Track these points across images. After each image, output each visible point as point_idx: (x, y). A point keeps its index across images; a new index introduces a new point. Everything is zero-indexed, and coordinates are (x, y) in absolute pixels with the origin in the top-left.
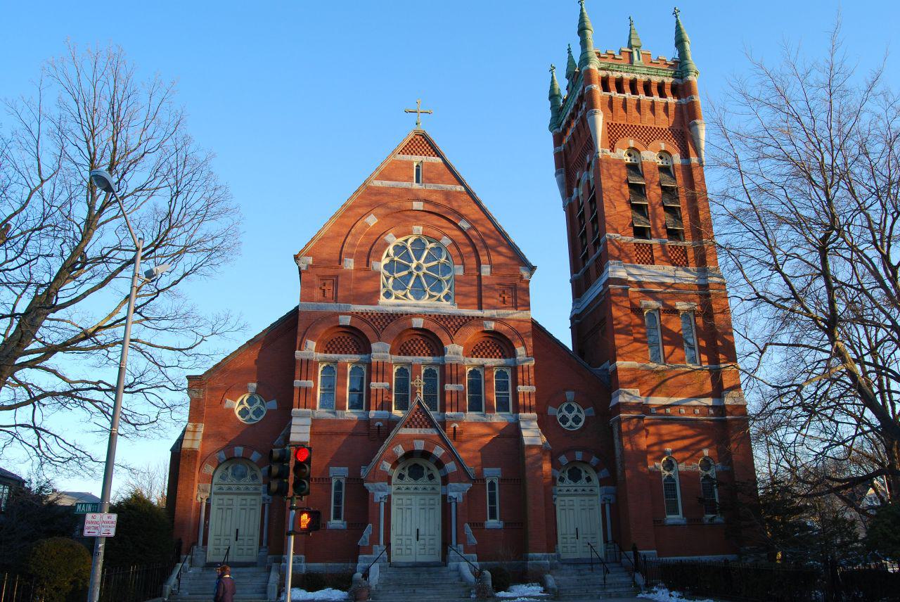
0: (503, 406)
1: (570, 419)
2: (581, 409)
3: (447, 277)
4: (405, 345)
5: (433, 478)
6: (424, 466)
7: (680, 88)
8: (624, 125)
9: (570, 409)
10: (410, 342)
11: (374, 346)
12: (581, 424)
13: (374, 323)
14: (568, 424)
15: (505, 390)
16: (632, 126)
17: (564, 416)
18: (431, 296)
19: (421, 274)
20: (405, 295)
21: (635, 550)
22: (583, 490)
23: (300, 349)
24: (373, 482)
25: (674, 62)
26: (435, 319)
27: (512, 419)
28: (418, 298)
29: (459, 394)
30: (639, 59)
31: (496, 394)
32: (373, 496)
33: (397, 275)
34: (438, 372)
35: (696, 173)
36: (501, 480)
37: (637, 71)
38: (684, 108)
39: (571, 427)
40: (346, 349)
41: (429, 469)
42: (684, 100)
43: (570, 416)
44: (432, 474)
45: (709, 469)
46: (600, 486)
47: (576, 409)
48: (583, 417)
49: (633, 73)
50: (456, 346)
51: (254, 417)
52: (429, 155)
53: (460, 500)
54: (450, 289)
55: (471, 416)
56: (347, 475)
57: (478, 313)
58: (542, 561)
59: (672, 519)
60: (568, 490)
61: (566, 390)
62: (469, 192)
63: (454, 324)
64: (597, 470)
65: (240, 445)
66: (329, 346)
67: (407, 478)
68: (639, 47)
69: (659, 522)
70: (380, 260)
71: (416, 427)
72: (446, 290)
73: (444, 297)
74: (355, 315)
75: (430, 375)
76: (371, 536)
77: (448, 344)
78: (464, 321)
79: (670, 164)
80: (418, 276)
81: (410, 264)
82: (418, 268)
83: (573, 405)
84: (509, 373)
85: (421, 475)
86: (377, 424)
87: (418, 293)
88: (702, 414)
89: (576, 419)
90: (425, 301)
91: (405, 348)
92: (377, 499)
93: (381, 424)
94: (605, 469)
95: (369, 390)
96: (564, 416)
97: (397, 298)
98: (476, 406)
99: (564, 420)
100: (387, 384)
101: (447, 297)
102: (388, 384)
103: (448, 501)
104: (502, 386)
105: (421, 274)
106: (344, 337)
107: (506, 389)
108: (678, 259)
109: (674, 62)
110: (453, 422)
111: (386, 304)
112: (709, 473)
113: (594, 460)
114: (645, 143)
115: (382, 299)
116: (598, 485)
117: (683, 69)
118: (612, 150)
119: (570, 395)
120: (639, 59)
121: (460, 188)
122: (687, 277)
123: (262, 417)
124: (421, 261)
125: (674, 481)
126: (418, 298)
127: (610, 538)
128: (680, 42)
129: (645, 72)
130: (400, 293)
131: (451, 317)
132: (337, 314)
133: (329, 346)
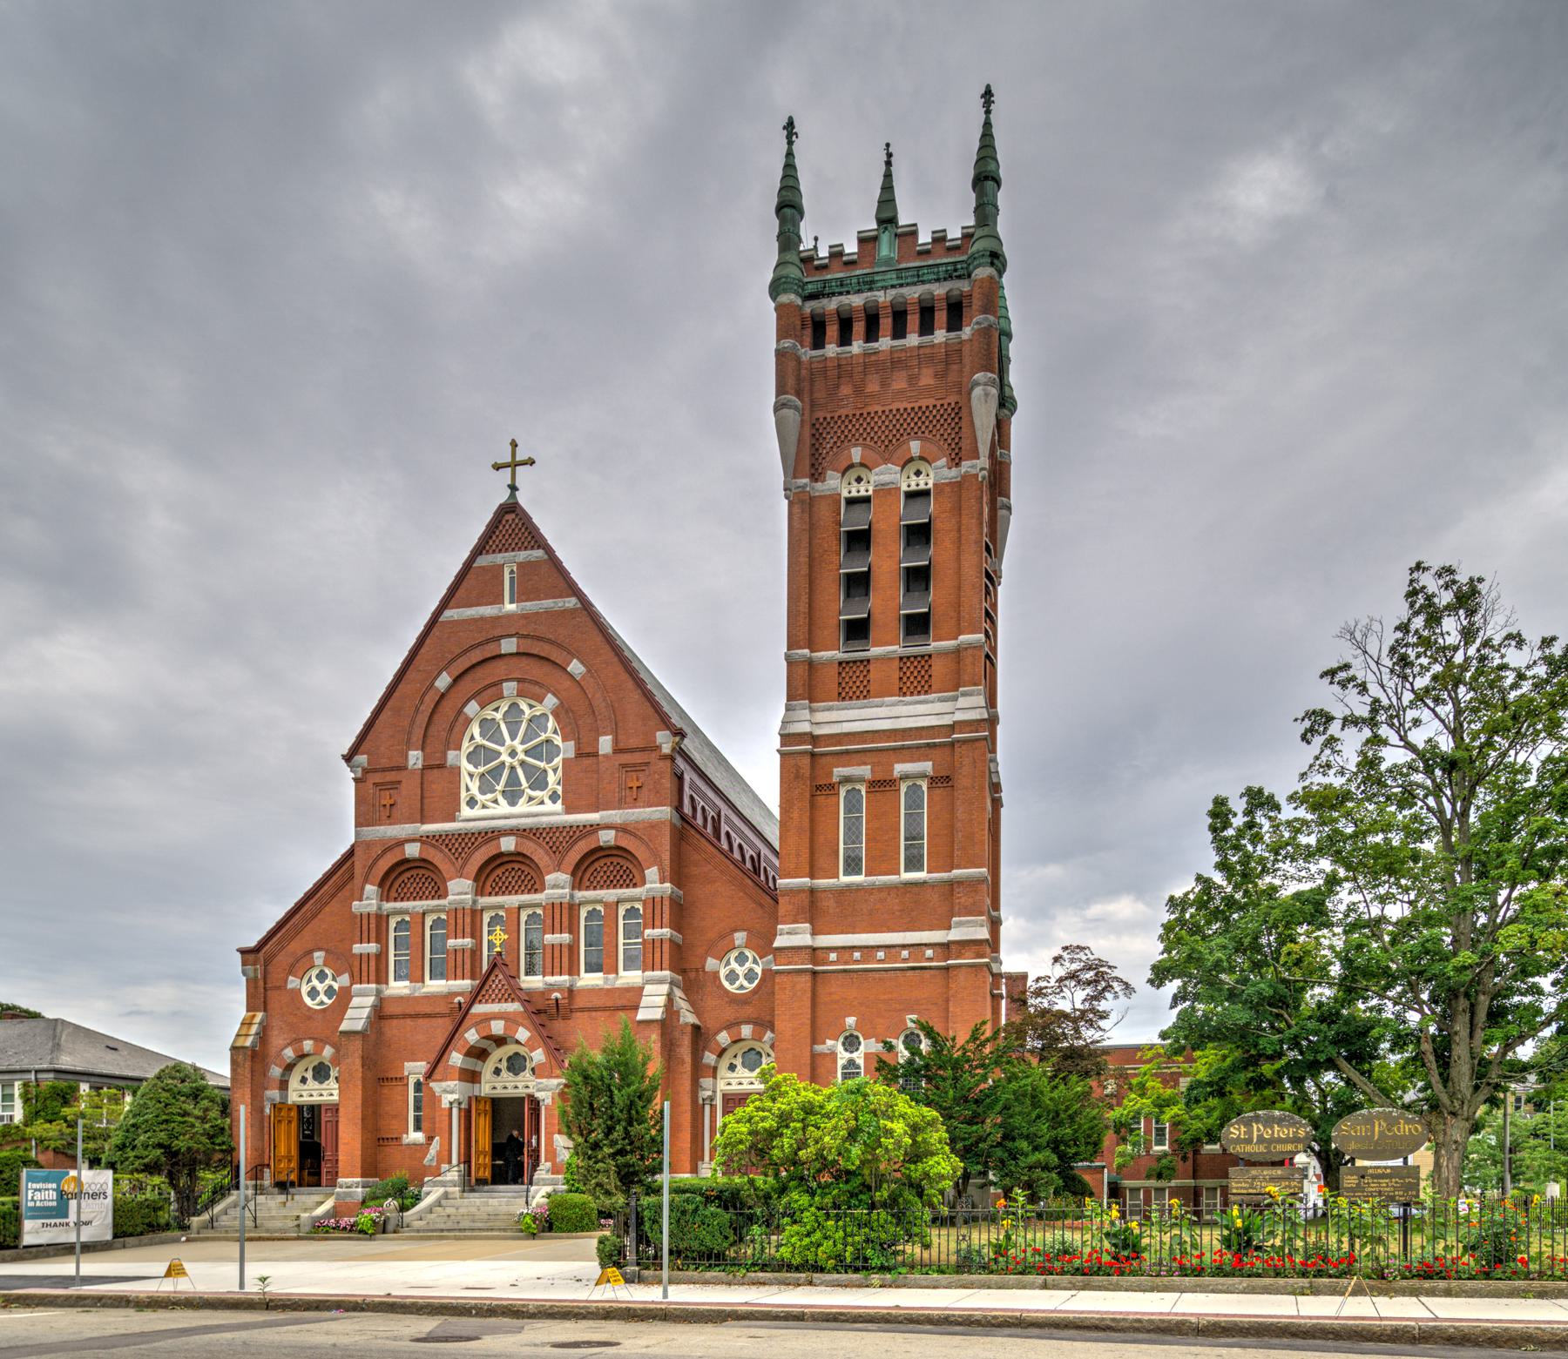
9: (741, 959)
16: (832, 418)
18: (531, 799)
19: (521, 756)
32: (440, 1101)
37: (879, 284)
39: (742, 987)
47: (751, 959)
51: (746, 984)
53: (549, 1101)
61: (736, 930)
65: (310, 1038)
67: (505, 1074)
76: (439, 1153)
80: (522, 763)
82: (513, 754)
85: (327, 1077)
86: (456, 1000)
87: (512, 796)
90: (522, 807)
92: (445, 1104)
93: (462, 1000)
96: (732, 971)
97: (484, 807)
99: (732, 976)
100: (565, 937)
101: (554, 797)
102: (565, 937)
105: (521, 756)
110: (554, 991)
111: (470, 817)
112: (855, 1055)
115: (466, 811)
119: (740, 937)
123: (756, 982)
124: (508, 741)
126: (513, 803)
128: (985, 179)
129: (895, 282)
131: (553, 830)
132: (401, 843)
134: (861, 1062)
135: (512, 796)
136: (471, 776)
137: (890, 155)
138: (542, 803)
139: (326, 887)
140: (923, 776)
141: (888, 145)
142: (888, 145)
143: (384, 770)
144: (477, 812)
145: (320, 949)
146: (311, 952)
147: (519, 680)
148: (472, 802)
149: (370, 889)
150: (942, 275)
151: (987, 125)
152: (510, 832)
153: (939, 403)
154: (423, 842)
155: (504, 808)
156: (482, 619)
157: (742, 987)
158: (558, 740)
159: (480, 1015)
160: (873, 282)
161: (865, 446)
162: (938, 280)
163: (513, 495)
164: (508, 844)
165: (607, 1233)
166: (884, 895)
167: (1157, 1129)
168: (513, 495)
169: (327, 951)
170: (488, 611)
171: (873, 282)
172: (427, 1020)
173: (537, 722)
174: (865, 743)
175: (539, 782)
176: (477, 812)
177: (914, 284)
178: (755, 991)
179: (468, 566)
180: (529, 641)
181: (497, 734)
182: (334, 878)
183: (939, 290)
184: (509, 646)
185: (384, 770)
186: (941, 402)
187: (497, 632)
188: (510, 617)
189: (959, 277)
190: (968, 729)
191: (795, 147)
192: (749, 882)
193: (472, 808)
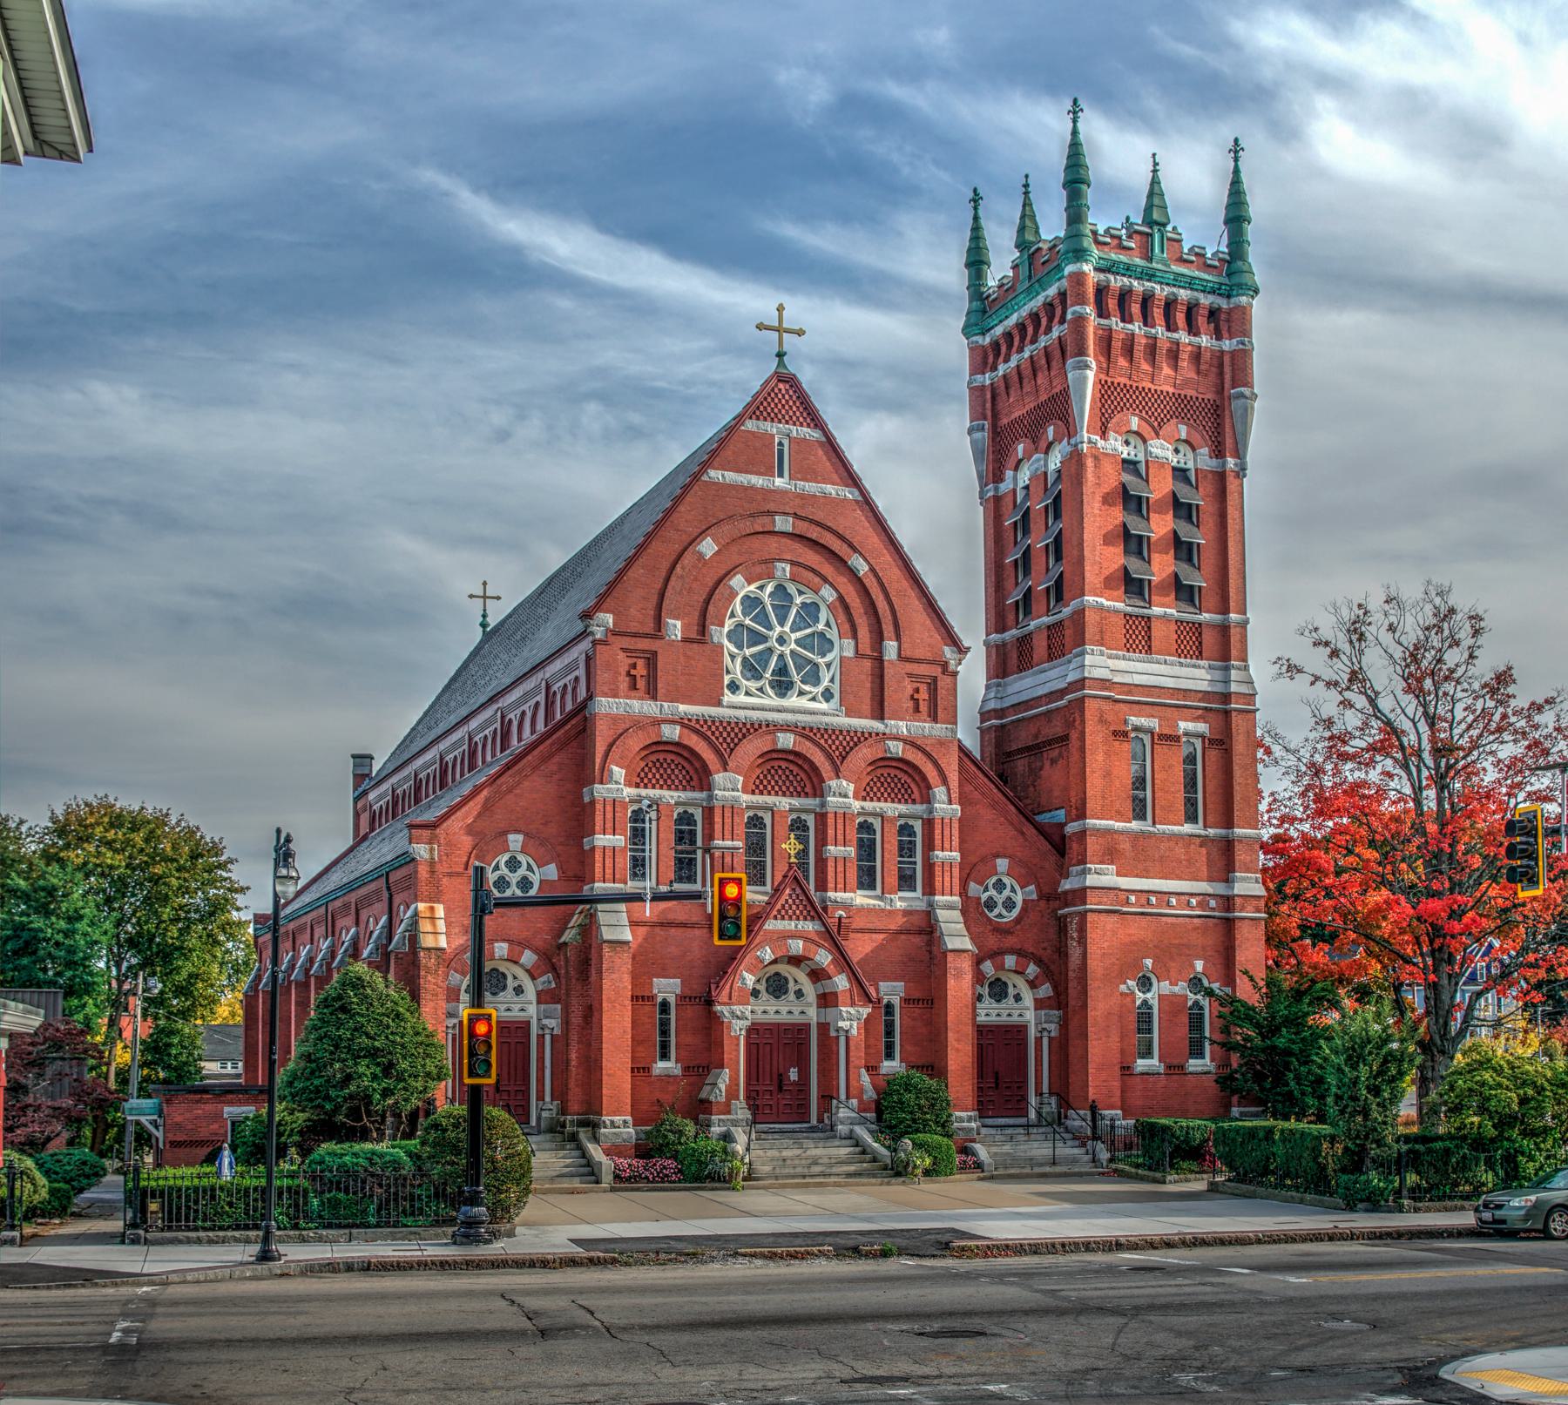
0: (906, 881)
1: (1000, 905)
2: (1017, 887)
3: (829, 657)
4: (761, 777)
5: (522, 992)
6: (506, 972)
7: (1223, 316)
8: (1125, 385)
9: (1000, 886)
10: (769, 771)
11: (719, 778)
12: (1015, 913)
13: (830, 746)
14: (996, 911)
15: (910, 856)
17: (502, 878)
18: (801, 693)
20: (761, 690)
21: (1094, 1109)
22: (765, 1012)
23: (602, 783)
24: (728, 1004)
25: (1220, 260)
26: (698, 726)
27: (921, 905)
28: (782, 695)
29: (848, 864)
30: (1163, 252)
31: (915, 863)
32: (729, 1028)
33: (748, 652)
34: (698, 817)
35: (1232, 484)
36: (906, 1001)
38: (1227, 359)
39: (1000, 916)
40: (669, 782)
41: (796, 981)
42: (1227, 342)
43: (514, 878)
44: (800, 990)
45: (1149, 990)
46: (1036, 1009)
47: (525, 865)
48: (1019, 899)
49: (1149, 280)
50: (844, 783)
51: (1004, 912)
52: (801, 425)
54: (832, 680)
55: (861, 898)
56: (678, 991)
57: (877, 726)
58: (965, 1124)
59: (1141, 1064)
60: (1009, 1015)
61: (998, 856)
62: (867, 503)
63: (840, 745)
64: (1033, 985)
65: (504, 940)
66: (642, 774)
67: (764, 995)
68: (1164, 225)
69: (1126, 1070)
70: (722, 625)
71: (790, 918)
72: (825, 683)
73: (822, 694)
74: (685, 723)
75: (755, 826)
77: (718, 772)
78: (855, 739)
79: (1141, 457)
81: (771, 633)
83: (521, 858)
84: (698, 817)
87: (783, 686)
88: (1200, 905)
89: (1009, 904)
90: (793, 701)
91: (761, 782)
94: (1048, 985)
95: (821, 862)
96: (502, 878)
97: (747, 694)
98: (867, 880)
101: (827, 695)
103: (833, 1034)
104: (906, 849)
106: (665, 759)
107: (912, 853)
108: (1191, 643)
109: (1220, 260)
110: (839, 909)
112: (1149, 995)
113: (1032, 970)
114: (1156, 424)
115: (728, 697)
116: (535, 1002)
117: (1235, 280)
118: (1104, 435)
119: (1002, 864)
120: (1163, 252)
121: (849, 494)
122: (1197, 676)
125: (1150, 1008)
127: (1045, 1089)
130: (753, 685)
132: (657, 722)
133: (642, 774)
134: (1155, 1003)
135: (783, 686)
136: (733, 657)
137: (1156, 164)
138: (813, 699)
139: (529, 757)
140: (1197, 735)
141: (1154, 155)
142: (1154, 155)
143: (635, 635)
144: (741, 698)
145: (517, 831)
146: (505, 833)
147: (793, 563)
148: (734, 687)
149: (618, 772)
150: (1208, 289)
151: (1236, 171)
152: (787, 728)
153: (1200, 396)
154: (683, 725)
155: (773, 700)
156: (753, 488)
157: (1000, 916)
158: (833, 634)
159: (773, 932)
160: (1154, 276)
161: (1141, 418)
162: (1203, 291)
163: (781, 364)
164: (786, 740)
165: (98, 1039)
166: (1172, 844)
167: (1150, 1031)
168: (781, 364)
169: (527, 835)
170: (758, 481)
171: (1154, 276)
172: (681, 930)
173: (811, 611)
174: (1152, 697)
175: (813, 678)
176: (741, 698)
177: (1184, 288)
178: (1018, 920)
179: (732, 429)
180: (806, 524)
181: (802, 625)
182: (541, 748)
183: (1184, 294)
184: (783, 523)
185: (635, 635)
186: (1200, 396)
187: (772, 507)
188: (783, 493)
189: (1220, 295)
190: (1242, 700)
191: (1232, 164)
192: (1013, 808)
193: (733, 693)
